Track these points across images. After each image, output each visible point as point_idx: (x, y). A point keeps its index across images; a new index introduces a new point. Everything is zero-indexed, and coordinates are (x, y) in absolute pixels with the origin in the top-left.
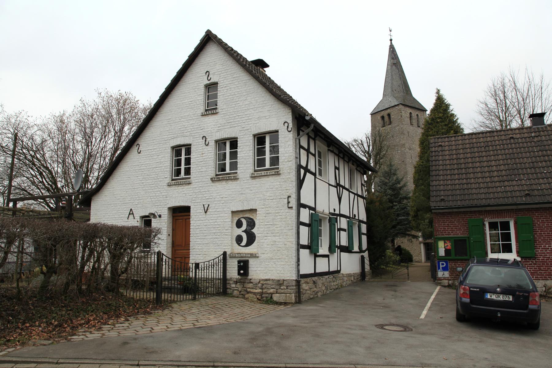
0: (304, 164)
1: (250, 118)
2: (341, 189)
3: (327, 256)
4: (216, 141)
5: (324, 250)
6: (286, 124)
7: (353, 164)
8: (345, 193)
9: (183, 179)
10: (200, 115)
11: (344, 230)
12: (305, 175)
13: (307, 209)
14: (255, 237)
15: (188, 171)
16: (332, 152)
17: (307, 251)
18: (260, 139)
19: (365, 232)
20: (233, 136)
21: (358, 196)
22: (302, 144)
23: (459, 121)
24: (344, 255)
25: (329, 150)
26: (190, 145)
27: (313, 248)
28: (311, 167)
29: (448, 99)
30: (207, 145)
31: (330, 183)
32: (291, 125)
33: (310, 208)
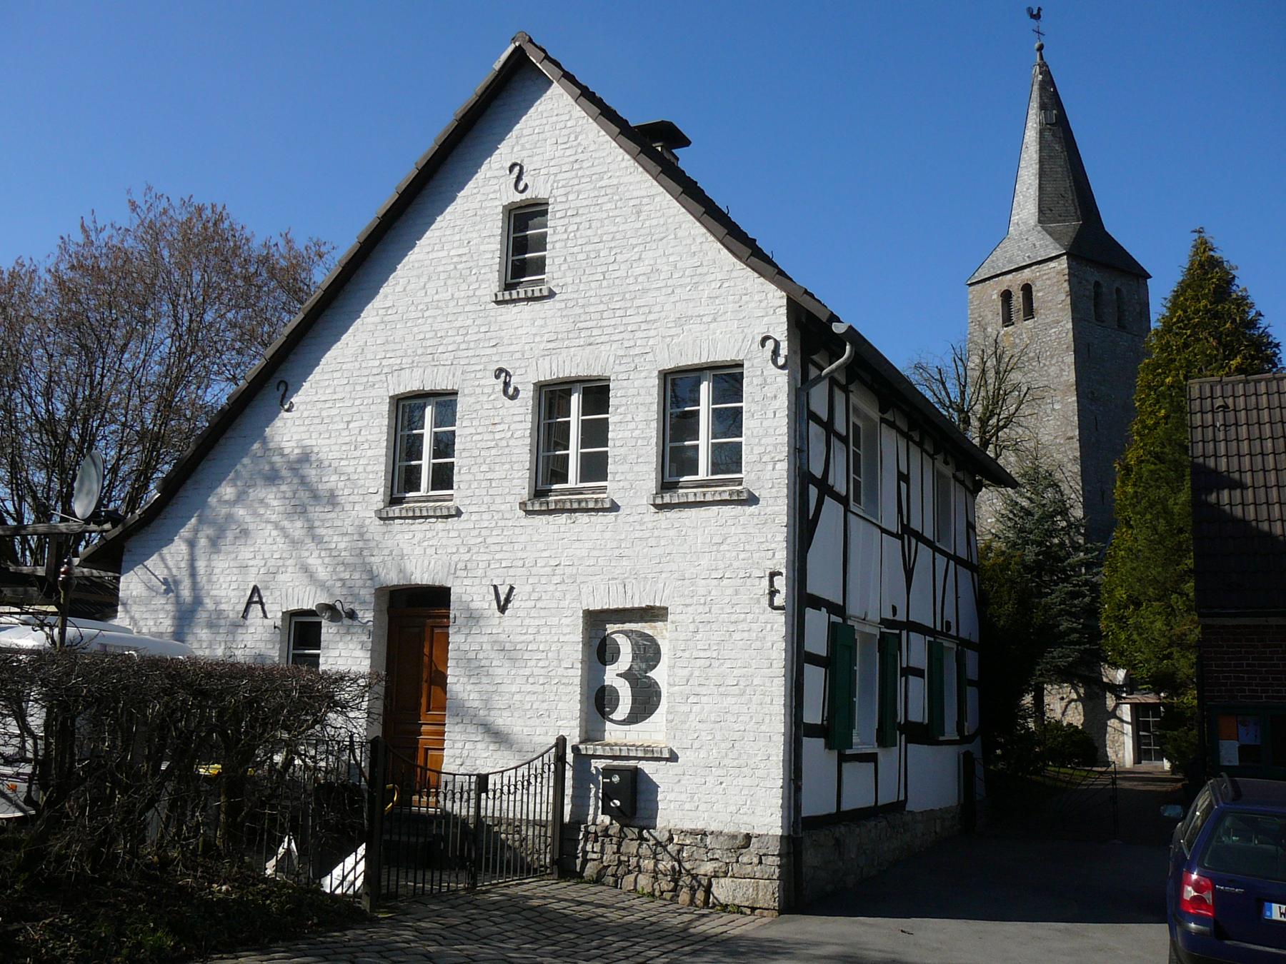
0: (817, 470)
1: (651, 317)
2: (913, 541)
3: (872, 758)
4: (540, 387)
5: (863, 737)
6: (770, 345)
7: (946, 463)
8: (925, 553)
9: (428, 499)
10: (488, 299)
11: (918, 673)
12: (820, 503)
13: (824, 610)
14: (658, 694)
15: (443, 478)
16: (892, 425)
17: (820, 742)
18: (677, 386)
19: (975, 678)
20: (595, 372)
21: (958, 561)
22: (813, 407)
23: (1263, 323)
24: (918, 752)
25: (883, 420)
26: (455, 393)
27: (834, 731)
28: (838, 481)
29: (1224, 252)
30: (513, 398)
31: (883, 526)
32: (784, 351)
33: (833, 608)
